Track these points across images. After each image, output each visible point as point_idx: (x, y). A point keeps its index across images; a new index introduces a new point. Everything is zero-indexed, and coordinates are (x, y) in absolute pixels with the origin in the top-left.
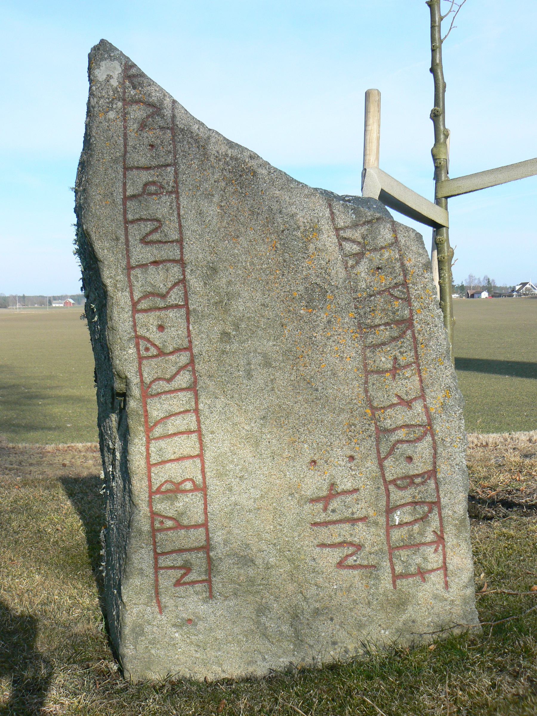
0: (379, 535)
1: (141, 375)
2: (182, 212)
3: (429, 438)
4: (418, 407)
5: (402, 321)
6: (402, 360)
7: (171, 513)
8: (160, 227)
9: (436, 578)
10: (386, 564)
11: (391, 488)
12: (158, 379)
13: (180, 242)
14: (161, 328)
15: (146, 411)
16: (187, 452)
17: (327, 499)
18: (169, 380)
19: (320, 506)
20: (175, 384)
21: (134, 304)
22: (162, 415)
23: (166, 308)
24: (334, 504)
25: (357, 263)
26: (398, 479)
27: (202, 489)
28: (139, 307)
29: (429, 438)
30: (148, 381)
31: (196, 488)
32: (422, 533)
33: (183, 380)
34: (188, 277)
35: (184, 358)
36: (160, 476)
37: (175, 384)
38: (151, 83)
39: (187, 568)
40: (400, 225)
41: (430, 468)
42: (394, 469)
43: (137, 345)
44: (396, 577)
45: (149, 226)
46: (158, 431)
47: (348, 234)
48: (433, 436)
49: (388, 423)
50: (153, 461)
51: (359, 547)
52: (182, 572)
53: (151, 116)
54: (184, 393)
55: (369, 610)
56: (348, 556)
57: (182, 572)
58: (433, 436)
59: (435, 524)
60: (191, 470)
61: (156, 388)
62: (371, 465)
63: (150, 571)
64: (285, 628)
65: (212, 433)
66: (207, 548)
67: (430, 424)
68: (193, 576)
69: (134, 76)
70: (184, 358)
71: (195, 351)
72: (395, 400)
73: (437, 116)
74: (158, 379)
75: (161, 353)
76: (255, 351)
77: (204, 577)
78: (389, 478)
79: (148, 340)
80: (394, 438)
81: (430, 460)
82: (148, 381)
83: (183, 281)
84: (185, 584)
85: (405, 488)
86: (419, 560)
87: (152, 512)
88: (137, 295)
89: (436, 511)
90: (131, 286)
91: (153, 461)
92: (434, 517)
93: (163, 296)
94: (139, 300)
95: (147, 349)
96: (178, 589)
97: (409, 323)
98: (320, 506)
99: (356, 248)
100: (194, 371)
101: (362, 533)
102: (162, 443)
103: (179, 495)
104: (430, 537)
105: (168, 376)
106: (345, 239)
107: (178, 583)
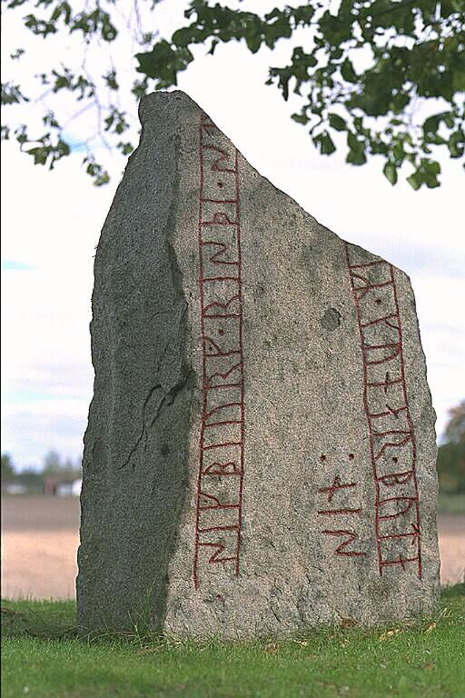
0: (370, 526)
1: (205, 370)
2: (241, 241)
3: (410, 443)
4: (402, 415)
5: (393, 345)
6: (392, 378)
7: (215, 494)
8: (224, 251)
9: (414, 566)
10: (375, 552)
11: (381, 483)
12: (217, 374)
13: (239, 264)
14: (221, 332)
15: (205, 401)
16: (232, 439)
17: (332, 490)
18: (224, 377)
19: (326, 496)
20: (229, 380)
21: (203, 311)
22: (217, 405)
23: (226, 317)
24: (337, 497)
25: (364, 295)
26: (386, 477)
27: (240, 473)
28: (207, 314)
29: (410, 443)
30: (209, 375)
31: (236, 472)
32: (403, 526)
33: (234, 377)
34: (243, 293)
35: (236, 359)
36: (211, 458)
37: (229, 380)
38: (220, 133)
39: (221, 546)
40: (396, 268)
41: (410, 469)
42: (383, 467)
43: (204, 345)
44: (382, 564)
45: (218, 248)
46: (212, 419)
47: (358, 271)
48: (413, 441)
49: (380, 429)
50: (205, 446)
51: (354, 536)
52: (218, 549)
53: (222, 159)
54: (234, 388)
55: (359, 595)
56: (345, 544)
57: (218, 549)
58: (413, 441)
59: (413, 519)
60: (232, 454)
61: (214, 382)
62: (366, 463)
63: (192, 546)
64: (293, 609)
65: (252, 424)
66: (239, 526)
67: (411, 432)
68: (225, 554)
69: (208, 125)
70: (236, 359)
71: (244, 354)
72: (387, 410)
73: (77, 114)
74: (217, 374)
75: (221, 354)
76: (287, 359)
77: (233, 555)
78: (380, 476)
79: (212, 341)
80: (384, 441)
81: (410, 463)
82: (209, 375)
83: (239, 296)
84: (218, 561)
85: (392, 484)
86: (400, 549)
87: (199, 491)
88: (206, 304)
89: (414, 504)
90: (202, 295)
91: (205, 446)
92: (413, 511)
93: (225, 307)
94: (207, 309)
95: (211, 349)
96: (214, 565)
97: (398, 348)
98: (326, 496)
99: (363, 284)
100: (242, 371)
101: (353, 523)
102: (215, 430)
103: (223, 477)
104: (409, 530)
105: (224, 373)
106: (358, 276)
107: (212, 560)
